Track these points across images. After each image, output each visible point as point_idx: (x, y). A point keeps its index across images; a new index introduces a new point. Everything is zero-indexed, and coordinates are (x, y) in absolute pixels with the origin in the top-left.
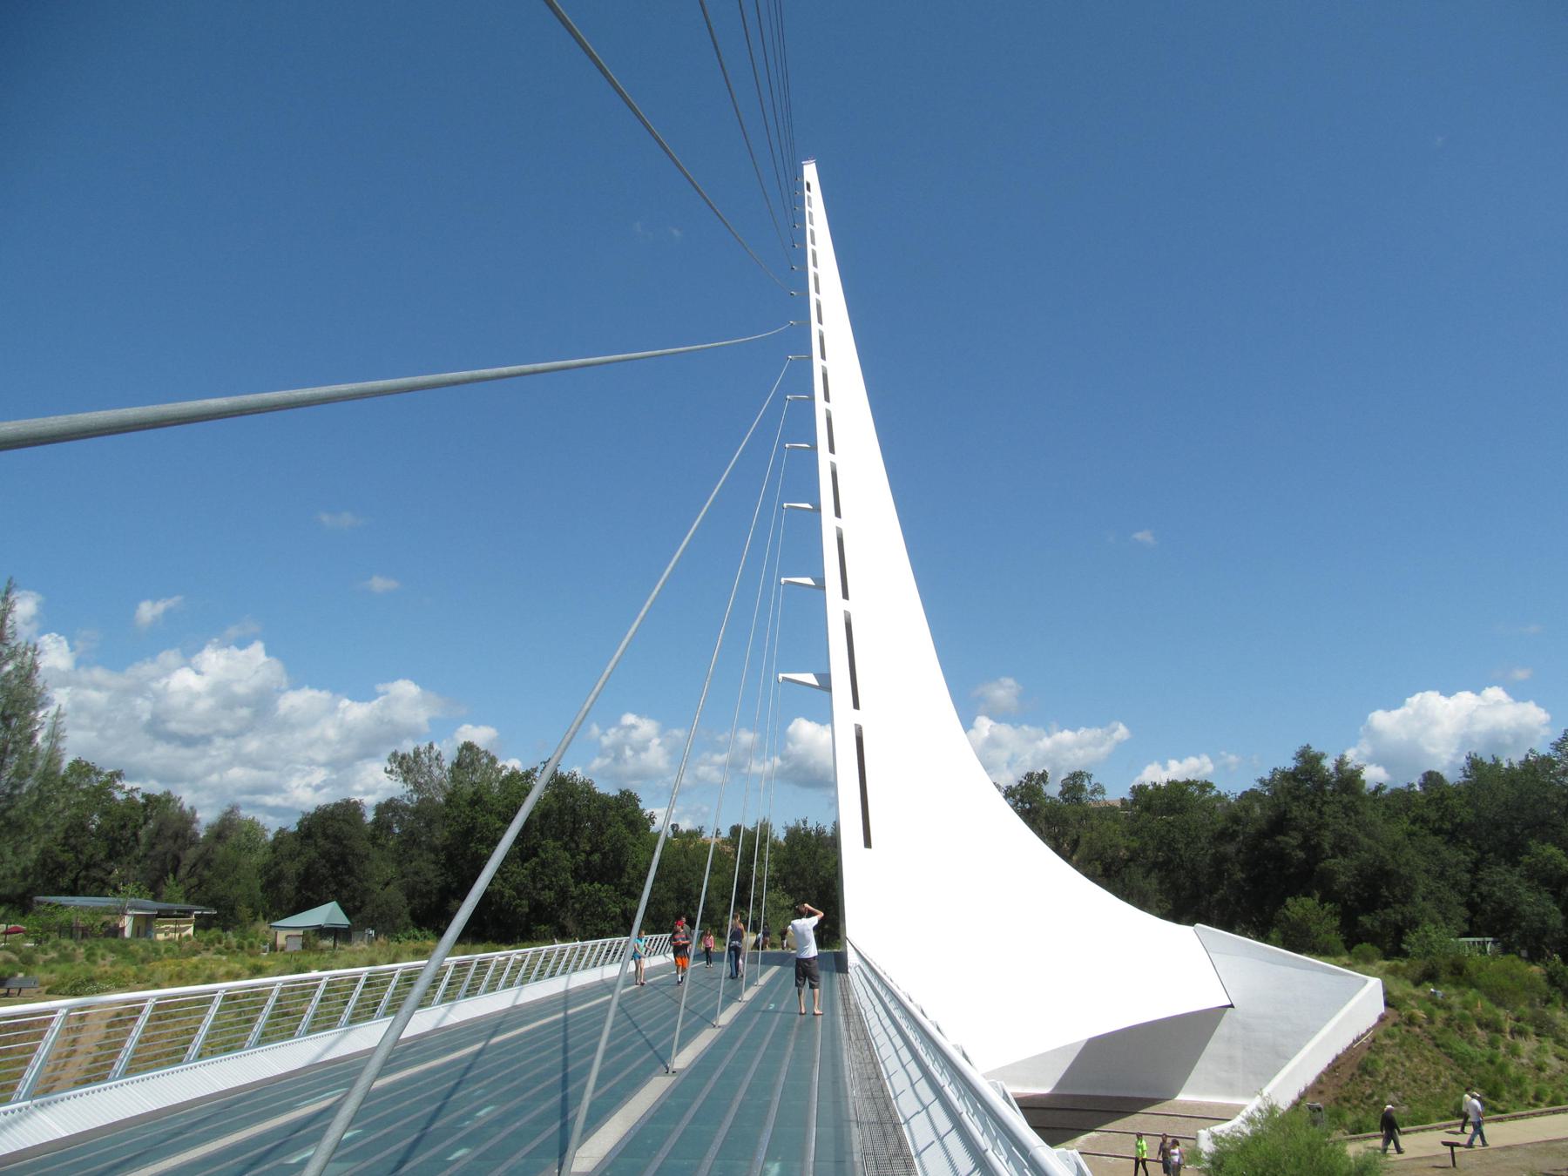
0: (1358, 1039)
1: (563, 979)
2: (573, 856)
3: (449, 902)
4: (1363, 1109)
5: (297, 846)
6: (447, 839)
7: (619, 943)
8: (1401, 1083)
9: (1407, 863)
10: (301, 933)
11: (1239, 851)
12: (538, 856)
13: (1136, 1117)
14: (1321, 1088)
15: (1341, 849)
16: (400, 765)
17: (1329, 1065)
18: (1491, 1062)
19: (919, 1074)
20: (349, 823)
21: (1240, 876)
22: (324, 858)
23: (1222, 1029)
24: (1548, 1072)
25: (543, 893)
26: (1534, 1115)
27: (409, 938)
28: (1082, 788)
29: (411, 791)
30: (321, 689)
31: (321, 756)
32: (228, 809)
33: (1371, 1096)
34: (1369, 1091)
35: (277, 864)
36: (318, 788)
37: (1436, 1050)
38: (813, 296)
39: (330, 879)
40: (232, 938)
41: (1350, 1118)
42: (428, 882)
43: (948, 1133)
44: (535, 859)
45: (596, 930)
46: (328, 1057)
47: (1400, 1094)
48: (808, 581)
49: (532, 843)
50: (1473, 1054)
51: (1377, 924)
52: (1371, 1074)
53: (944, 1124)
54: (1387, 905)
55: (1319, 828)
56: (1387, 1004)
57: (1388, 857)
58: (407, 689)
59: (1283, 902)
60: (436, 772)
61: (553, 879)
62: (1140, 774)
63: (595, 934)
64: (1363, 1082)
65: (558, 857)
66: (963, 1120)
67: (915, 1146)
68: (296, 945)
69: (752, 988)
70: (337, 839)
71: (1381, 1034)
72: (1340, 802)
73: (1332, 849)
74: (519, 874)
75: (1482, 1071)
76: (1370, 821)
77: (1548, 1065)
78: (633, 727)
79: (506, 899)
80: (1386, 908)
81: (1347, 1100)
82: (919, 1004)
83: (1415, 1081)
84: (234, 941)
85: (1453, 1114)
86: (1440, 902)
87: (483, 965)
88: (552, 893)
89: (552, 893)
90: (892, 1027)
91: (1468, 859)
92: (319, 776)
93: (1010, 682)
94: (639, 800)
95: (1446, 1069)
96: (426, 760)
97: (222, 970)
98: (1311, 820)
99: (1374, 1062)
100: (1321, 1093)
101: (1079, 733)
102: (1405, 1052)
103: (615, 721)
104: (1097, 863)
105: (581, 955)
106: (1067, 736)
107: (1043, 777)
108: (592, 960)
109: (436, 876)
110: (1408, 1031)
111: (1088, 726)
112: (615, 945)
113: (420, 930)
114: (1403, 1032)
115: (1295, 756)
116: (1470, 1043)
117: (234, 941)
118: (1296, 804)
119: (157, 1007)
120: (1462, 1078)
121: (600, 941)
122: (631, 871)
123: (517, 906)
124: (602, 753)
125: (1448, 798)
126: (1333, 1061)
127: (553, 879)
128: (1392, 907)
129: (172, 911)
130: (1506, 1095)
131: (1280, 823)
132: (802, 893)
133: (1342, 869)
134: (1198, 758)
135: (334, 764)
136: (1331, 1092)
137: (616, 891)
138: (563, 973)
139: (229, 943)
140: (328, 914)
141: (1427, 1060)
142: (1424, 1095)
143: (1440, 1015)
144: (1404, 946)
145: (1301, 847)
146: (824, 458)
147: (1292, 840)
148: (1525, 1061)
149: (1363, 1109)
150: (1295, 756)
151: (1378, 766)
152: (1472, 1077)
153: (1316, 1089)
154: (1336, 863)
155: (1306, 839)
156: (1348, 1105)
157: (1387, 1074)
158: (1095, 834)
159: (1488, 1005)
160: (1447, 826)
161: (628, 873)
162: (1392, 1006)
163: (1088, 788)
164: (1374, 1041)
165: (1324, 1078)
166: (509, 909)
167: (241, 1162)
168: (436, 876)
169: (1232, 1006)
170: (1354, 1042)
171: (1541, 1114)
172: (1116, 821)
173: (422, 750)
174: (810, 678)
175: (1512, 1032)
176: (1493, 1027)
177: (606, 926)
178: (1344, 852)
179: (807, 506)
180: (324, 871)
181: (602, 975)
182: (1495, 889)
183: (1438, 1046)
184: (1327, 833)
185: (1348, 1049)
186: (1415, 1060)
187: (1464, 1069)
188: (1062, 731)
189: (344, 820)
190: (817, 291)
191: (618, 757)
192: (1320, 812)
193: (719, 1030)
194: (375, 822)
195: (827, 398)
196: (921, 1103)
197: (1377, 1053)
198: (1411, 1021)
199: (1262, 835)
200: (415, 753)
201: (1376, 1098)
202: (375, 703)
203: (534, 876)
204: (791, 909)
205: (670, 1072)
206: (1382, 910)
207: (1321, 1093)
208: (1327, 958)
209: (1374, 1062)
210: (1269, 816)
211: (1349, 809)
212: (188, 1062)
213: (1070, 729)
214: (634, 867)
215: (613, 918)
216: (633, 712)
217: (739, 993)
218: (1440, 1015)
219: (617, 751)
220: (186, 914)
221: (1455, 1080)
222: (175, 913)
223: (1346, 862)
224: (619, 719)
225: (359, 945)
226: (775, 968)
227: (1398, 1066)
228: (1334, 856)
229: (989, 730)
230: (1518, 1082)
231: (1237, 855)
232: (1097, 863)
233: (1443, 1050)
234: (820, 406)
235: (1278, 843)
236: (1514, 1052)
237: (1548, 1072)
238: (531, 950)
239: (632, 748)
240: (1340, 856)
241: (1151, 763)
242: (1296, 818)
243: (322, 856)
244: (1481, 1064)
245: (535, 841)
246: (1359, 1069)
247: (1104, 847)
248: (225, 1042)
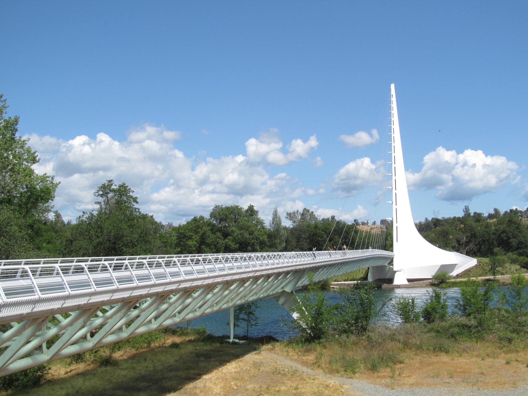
133: (514, 242)
136: (463, 273)
145: (506, 236)
178: (515, 238)
198: (480, 265)
199: (501, 233)
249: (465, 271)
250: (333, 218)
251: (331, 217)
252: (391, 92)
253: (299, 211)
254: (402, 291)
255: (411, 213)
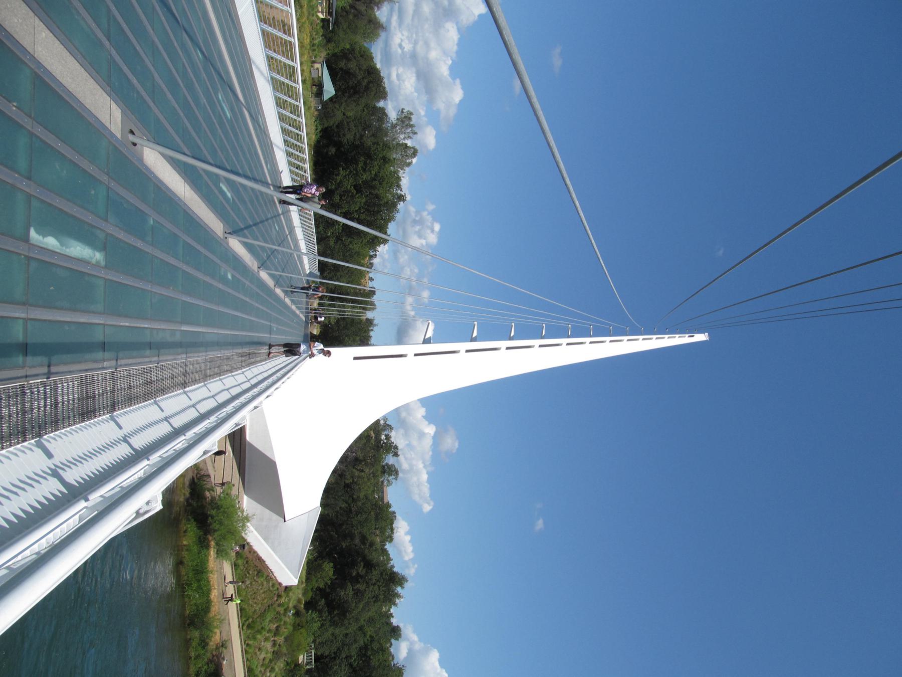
0: (271, 572)
1: (302, 238)
2: (356, 211)
3: (334, 147)
4: (243, 569)
5: (364, 67)
6: (367, 144)
7: (312, 228)
8: (254, 587)
9: (350, 624)
10: (320, 75)
11: (356, 546)
12: (357, 193)
13: (238, 475)
14: (252, 553)
15: (357, 593)
16: (405, 117)
17: (261, 557)
18: (262, 628)
19: (220, 401)
20: (375, 95)
21: (344, 545)
22: (358, 82)
23: (275, 517)
24: (258, 653)
25: (338, 196)
26: (241, 641)
27: (316, 126)
28: (390, 475)
29: (392, 123)
30: (458, 44)
31: (420, 48)
32: (384, 26)
33: (249, 573)
34: (250, 572)
35: (355, 58)
36: (400, 46)
37: (267, 606)
38: (641, 337)
39: (347, 86)
40: (319, 39)
41: (240, 562)
42: (344, 135)
43: (197, 411)
44: (355, 192)
45: (319, 224)
46: (254, 68)
47: (249, 586)
48: (512, 334)
49: (363, 190)
50: (265, 621)
51: (321, 607)
52: (257, 574)
53: (178, 422)
54: (330, 613)
55: (367, 583)
56: (286, 587)
57: (353, 615)
58: (457, 95)
59: (331, 562)
60: (402, 136)
61: (345, 202)
62: (403, 519)
63: (317, 223)
64: (254, 570)
65: (356, 203)
66: (204, 420)
67: (225, 378)
68: (314, 75)
69: (283, 295)
70: (367, 88)
71: (274, 582)
72: (380, 594)
73: (357, 589)
74: (348, 184)
75: (258, 623)
76: (370, 609)
77: (261, 653)
78: (433, 231)
79: (335, 177)
80: (328, 612)
81: (247, 562)
82: (274, 394)
83: (255, 593)
84: (316, 42)
85: (242, 607)
86: (331, 642)
87: (301, 150)
88: (338, 201)
89: (338, 201)
90: (275, 370)
91: (352, 661)
92: (408, 47)
93: (457, 445)
94: (385, 244)
95: (260, 608)
96: (409, 131)
97: (305, 68)
98: (371, 579)
99: (262, 576)
100: (250, 552)
101: (426, 484)
102: (267, 591)
103: (435, 219)
104: (351, 481)
105: (310, 227)
106: (425, 477)
107: (396, 455)
108: (305, 227)
109: (348, 140)
110: (275, 594)
111: (430, 489)
112: (309, 212)
113: (320, 132)
114: (275, 592)
115: (403, 574)
116: (270, 621)
117: (316, 42)
118: (379, 573)
119: (290, 42)
120: (256, 614)
121: (314, 227)
122: (349, 240)
123: (332, 183)
124: (418, 212)
125: (383, 654)
126: (263, 560)
127: (345, 202)
128: (328, 615)
129: (332, 9)
130: (249, 631)
131: (369, 565)
132: (337, 328)
133: (347, 593)
134: (413, 551)
135: (414, 56)
136: (250, 556)
137: (339, 233)
138: (304, 237)
139: (316, 40)
140: (329, 90)
141: (263, 600)
142: (249, 597)
143: (281, 610)
144: (310, 611)
146: (537, 342)
147: (361, 570)
148: (263, 643)
149: (243, 569)
150: (403, 574)
151: (407, 653)
152: (256, 619)
153: (252, 551)
154: (350, 590)
155: (361, 577)
156: (245, 563)
157: (257, 582)
158: (366, 480)
159: (286, 634)
160: (369, 653)
161: (347, 239)
162: (285, 590)
163: (390, 478)
164: (271, 578)
165: (256, 554)
166: (330, 179)
167: (219, 68)
168: (348, 140)
169: (285, 521)
170: (270, 570)
171: (241, 645)
172: (373, 491)
173: (414, 129)
174: (475, 334)
175: (274, 640)
176: (277, 632)
177: (321, 228)
179: (544, 334)
180: (351, 83)
181: (296, 227)
182: (338, 666)
183: (269, 606)
184: (364, 587)
185: (268, 567)
186: (263, 595)
187: (259, 616)
188: (427, 473)
189: (376, 92)
190: (628, 340)
191: (415, 222)
192: (374, 584)
193: (257, 271)
194: (375, 108)
195: (591, 343)
196: (250, 379)
197: (266, 578)
198: (279, 596)
200: (412, 125)
201: (248, 575)
202: (450, 79)
203: (347, 191)
204: (329, 322)
205: (226, 235)
206: (327, 611)
207: (250, 552)
208: (306, 563)
209: (262, 576)
210: (373, 560)
211: (376, 599)
212: (260, 25)
213: (428, 478)
214: (351, 242)
215: (325, 232)
216: (441, 230)
217: (280, 286)
218: (281, 610)
219: (420, 222)
220: (330, 14)
221: (255, 611)
222: (331, 11)
223: (351, 593)
224: (437, 221)
225: (313, 102)
226: (304, 319)
227: (260, 587)
228: (353, 590)
229: (428, 433)
230: (255, 638)
231: (354, 544)
232: (351, 481)
233: (267, 608)
234: (608, 339)
235: (360, 563)
236: (266, 639)
237: (258, 653)
238: (307, 157)
239: (420, 230)
240: (353, 592)
241: (409, 525)
242: (372, 572)
243: (359, 82)
244: (261, 624)
245: (364, 192)
246: (260, 570)
247: (359, 484)
248: (269, 41)
249: (260, 559)
250: (401, 198)
251: (403, 193)
252: (697, 333)
253: (415, 135)
254: (241, 378)
255: (450, 390)
